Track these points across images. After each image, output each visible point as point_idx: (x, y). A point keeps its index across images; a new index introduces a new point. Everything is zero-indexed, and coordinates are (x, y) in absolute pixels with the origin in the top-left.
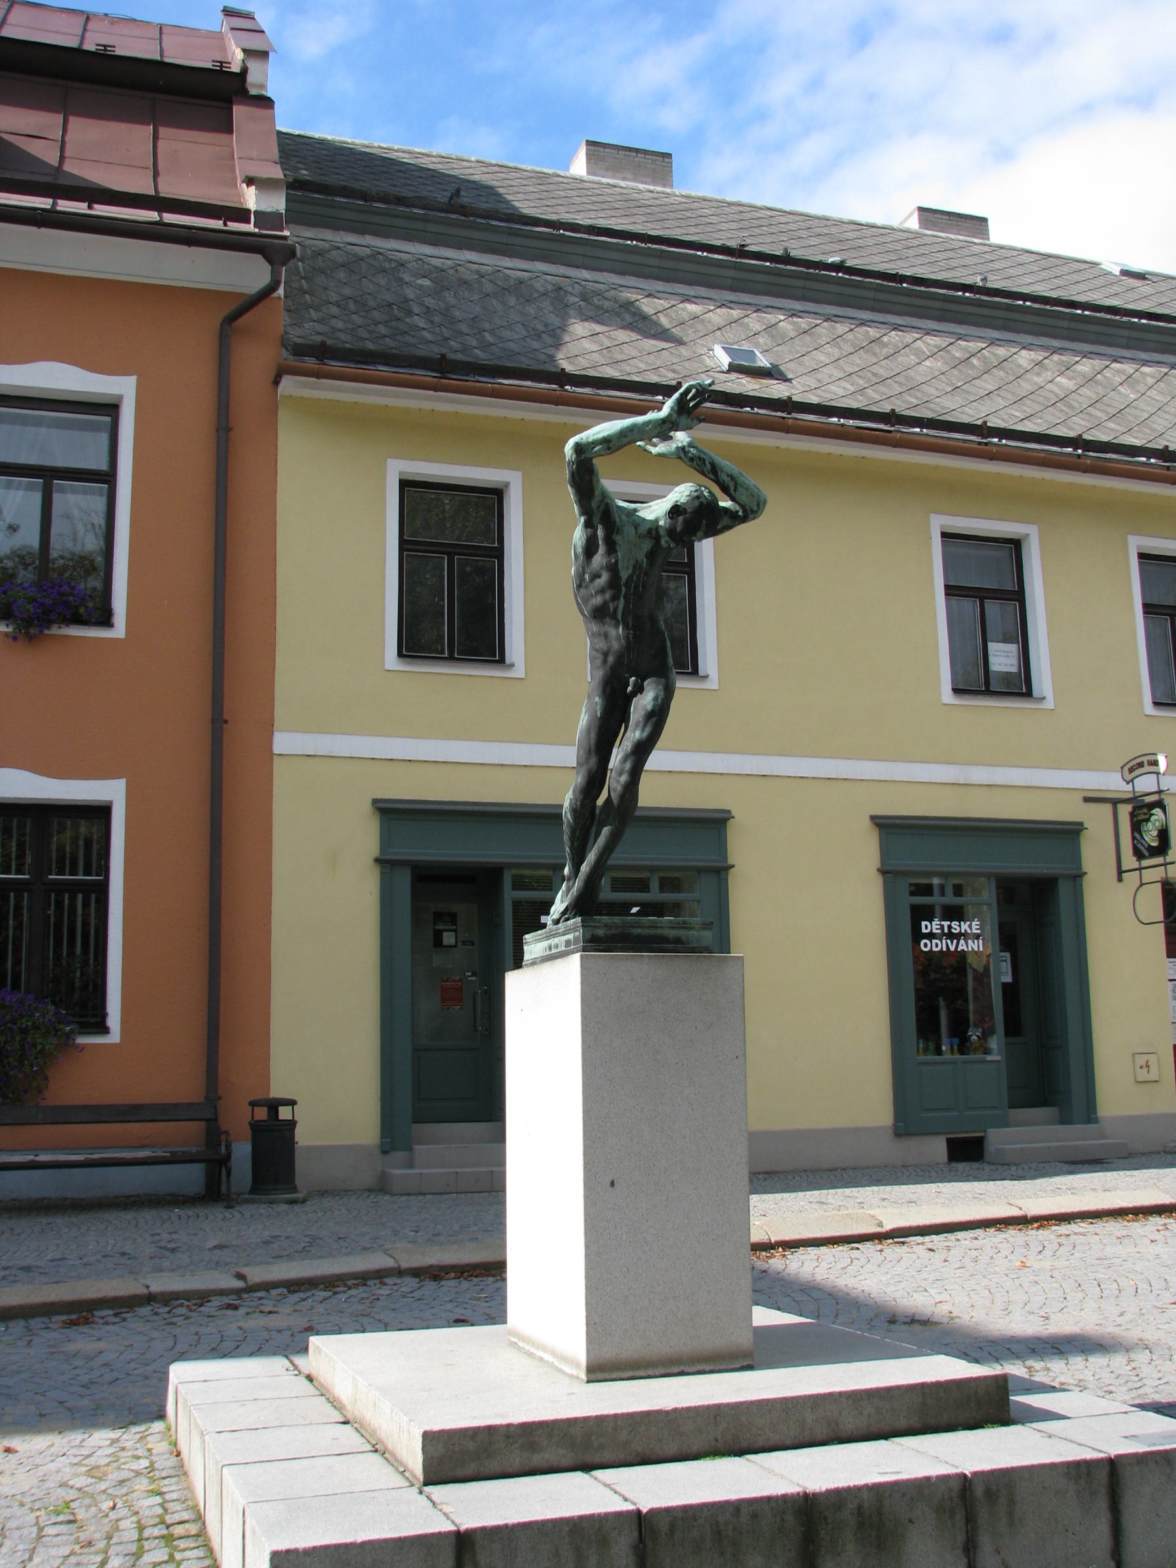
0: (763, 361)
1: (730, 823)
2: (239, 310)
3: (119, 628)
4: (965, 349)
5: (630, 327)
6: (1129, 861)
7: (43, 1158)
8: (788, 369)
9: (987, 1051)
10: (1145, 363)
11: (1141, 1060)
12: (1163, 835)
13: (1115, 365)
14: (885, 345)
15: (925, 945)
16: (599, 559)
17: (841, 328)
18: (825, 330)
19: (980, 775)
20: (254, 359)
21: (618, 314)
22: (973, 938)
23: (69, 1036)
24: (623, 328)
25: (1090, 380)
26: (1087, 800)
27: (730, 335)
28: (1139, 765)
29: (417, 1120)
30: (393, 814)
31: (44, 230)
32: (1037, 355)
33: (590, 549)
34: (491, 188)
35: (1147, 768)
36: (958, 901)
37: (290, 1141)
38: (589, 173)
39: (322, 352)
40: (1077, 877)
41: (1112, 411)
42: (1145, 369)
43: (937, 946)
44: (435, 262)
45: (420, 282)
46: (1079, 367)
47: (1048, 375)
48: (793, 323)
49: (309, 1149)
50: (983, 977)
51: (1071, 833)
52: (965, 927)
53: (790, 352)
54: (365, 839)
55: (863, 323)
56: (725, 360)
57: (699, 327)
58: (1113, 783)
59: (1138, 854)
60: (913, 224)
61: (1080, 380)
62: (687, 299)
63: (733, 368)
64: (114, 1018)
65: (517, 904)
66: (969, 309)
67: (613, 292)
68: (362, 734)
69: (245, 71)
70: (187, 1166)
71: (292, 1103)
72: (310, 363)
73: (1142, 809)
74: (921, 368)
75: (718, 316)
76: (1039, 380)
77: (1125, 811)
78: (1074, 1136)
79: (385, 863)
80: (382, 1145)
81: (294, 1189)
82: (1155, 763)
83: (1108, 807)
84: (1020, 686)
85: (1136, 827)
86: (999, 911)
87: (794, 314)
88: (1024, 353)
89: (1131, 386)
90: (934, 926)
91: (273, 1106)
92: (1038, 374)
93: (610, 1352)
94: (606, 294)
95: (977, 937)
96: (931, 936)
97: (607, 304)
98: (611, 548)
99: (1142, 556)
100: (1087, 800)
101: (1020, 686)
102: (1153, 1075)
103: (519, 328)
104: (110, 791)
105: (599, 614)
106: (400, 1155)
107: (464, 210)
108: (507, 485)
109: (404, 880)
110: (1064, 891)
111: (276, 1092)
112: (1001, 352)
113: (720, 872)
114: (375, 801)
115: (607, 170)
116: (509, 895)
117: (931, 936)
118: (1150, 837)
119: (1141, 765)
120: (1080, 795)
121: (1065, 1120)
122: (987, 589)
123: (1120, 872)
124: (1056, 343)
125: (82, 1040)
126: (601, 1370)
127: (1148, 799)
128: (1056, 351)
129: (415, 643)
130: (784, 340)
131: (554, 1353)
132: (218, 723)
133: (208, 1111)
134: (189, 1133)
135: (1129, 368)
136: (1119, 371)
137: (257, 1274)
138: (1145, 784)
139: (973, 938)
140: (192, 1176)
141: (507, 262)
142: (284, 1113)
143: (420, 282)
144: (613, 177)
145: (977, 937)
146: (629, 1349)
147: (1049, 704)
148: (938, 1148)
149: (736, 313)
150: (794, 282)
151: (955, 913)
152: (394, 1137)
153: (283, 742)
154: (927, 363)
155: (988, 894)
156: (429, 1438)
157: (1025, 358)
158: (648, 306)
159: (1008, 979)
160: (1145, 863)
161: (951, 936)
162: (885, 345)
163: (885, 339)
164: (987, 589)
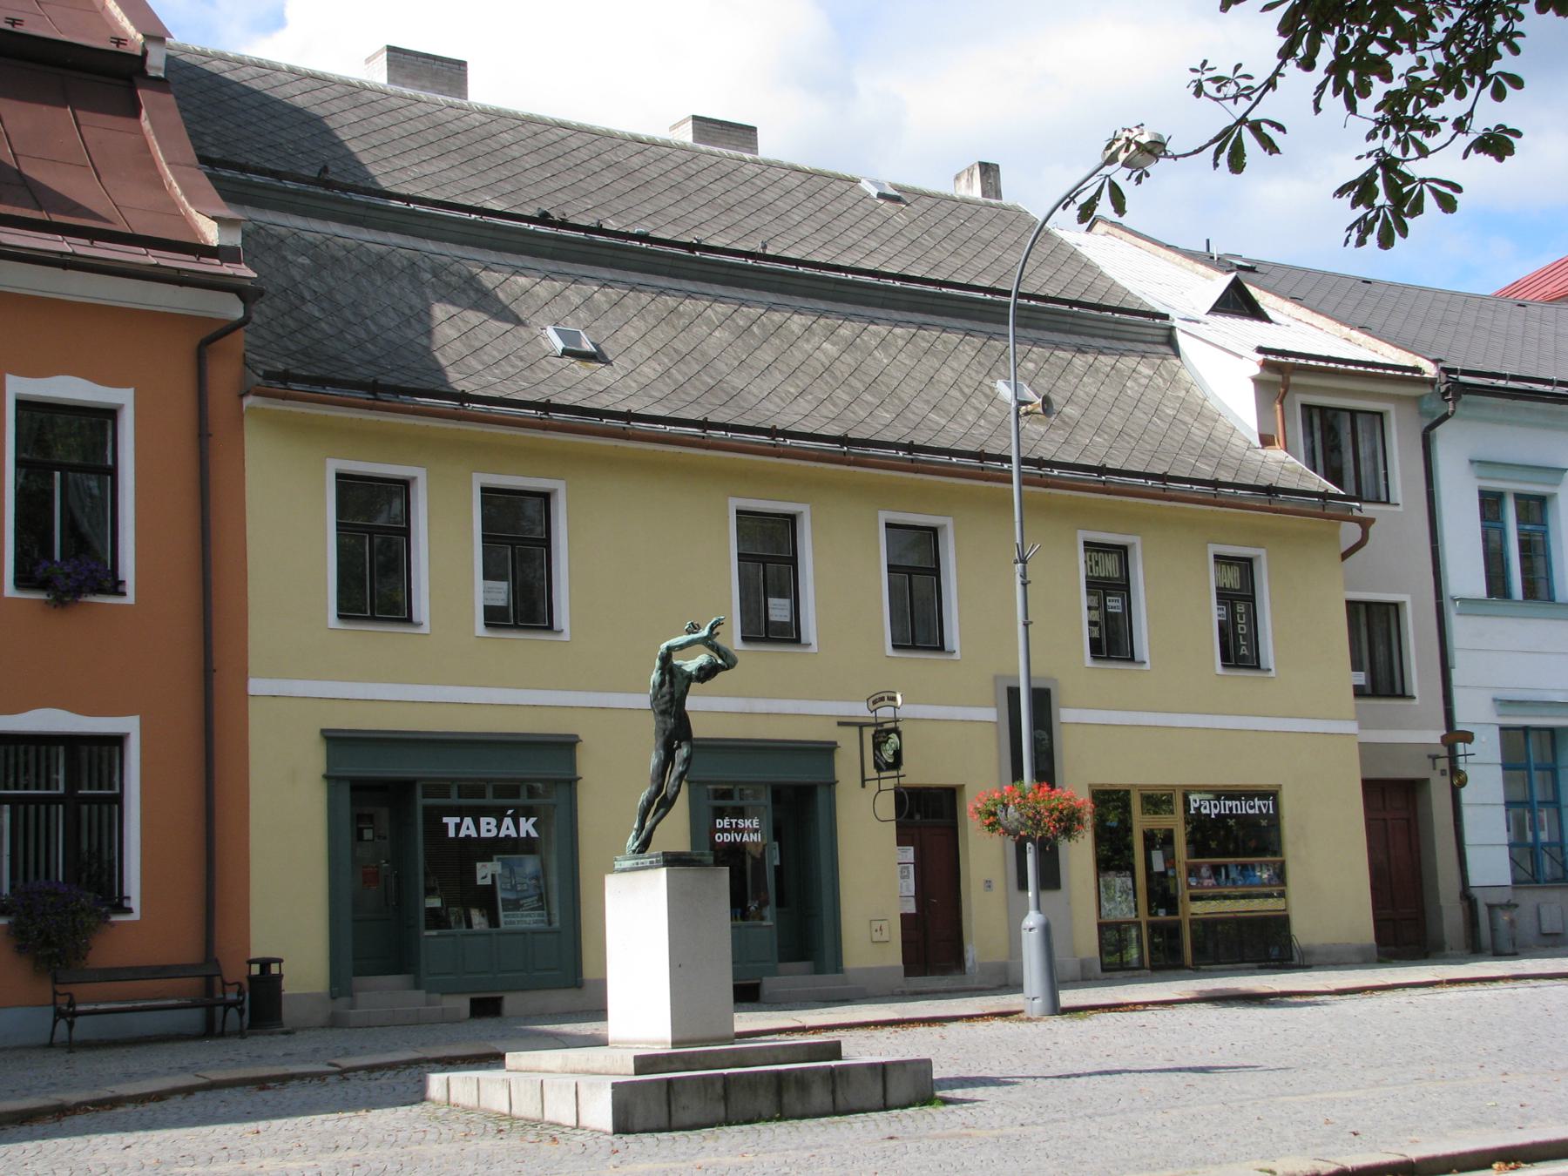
0: (588, 347)
1: (579, 746)
2: (213, 336)
3: (130, 598)
4: (747, 317)
5: (475, 307)
6: (871, 772)
7: (101, 1007)
8: (609, 349)
9: (762, 919)
10: (897, 324)
11: (876, 925)
12: (898, 754)
13: (872, 327)
14: (681, 315)
15: (721, 838)
16: (666, 689)
17: (645, 298)
18: (634, 301)
19: (761, 705)
20: (224, 373)
21: (464, 291)
22: (752, 831)
23: (108, 917)
24: (471, 308)
25: (850, 345)
26: (840, 724)
27: (556, 310)
28: (877, 700)
29: (356, 974)
30: (336, 741)
31: (70, 272)
32: (805, 320)
33: (662, 684)
34: (319, 119)
35: (886, 702)
36: (741, 803)
37: (279, 989)
38: (391, 80)
39: (285, 377)
40: (831, 785)
41: (868, 380)
42: (898, 331)
43: (727, 838)
44: (309, 236)
45: (300, 260)
46: (842, 331)
47: (816, 340)
48: (606, 295)
49: (293, 996)
50: (759, 863)
51: (826, 751)
52: (748, 823)
53: (606, 328)
54: (315, 760)
55: (662, 291)
56: (559, 345)
57: (530, 301)
58: (860, 710)
59: (878, 768)
60: (686, 136)
61: (842, 346)
62: (517, 271)
63: (565, 353)
64: (135, 903)
65: (426, 808)
66: (750, 274)
67: (456, 266)
68: (312, 679)
69: (145, 53)
70: (189, 1011)
71: (280, 961)
72: (278, 387)
73: (882, 733)
74: (712, 340)
75: (544, 289)
76: (808, 347)
77: (869, 733)
78: (826, 981)
79: (331, 779)
80: (331, 992)
81: (281, 1025)
82: (894, 699)
83: (856, 729)
84: (789, 634)
85: (877, 746)
86: (774, 810)
87: (604, 285)
88: (796, 317)
89: (885, 350)
90: (723, 823)
91: (265, 964)
92: (808, 341)
93: (679, 1037)
94: (452, 269)
95: (756, 831)
96: (723, 830)
97: (454, 279)
98: (672, 684)
99: (888, 525)
100: (840, 724)
101: (789, 634)
102: (885, 937)
103: (391, 314)
104: (128, 725)
105: (663, 713)
106: (343, 1001)
107: (329, 185)
108: (414, 478)
109: (345, 791)
110: (821, 794)
111: (256, 953)
112: (777, 317)
113: (571, 783)
114: (323, 731)
115: (407, 77)
116: (421, 802)
117: (723, 830)
118: (888, 754)
119: (882, 699)
120: (835, 721)
121: (818, 970)
122: (769, 556)
123: (864, 781)
124: (822, 305)
125: (114, 918)
126: (675, 1044)
127: (887, 726)
128: (822, 314)
129: (350, 609)
130: (598, 314)
131: (647, 1042)
132: (208, 672)
133: (208, 968)
134: (192, 984)
135: (882, 329)
136: (875, 334)
137: (347, 1062)
138: (885, 713)
139: (752, 831)
140: (195, 1017)
141: (366, 235)
142: (274, 969)
143: (300, 260)
144: (413, 87)
145: (756, 831)
146: (688, 1035)
147: (814, 648)
148: (462, 1004)
149: (558, 285)
150: (605, 252)
151: (740, 813)
152: (339, 984)
153: (256, 686)
154: (717, 334)
155: (766, 799)
156: (637, 1058)
157: (797, 322)
158: (489, 279)
159: (777, 862)
160: (883, 774)
161: (738, 831)
162: (681, 315)
163: (681, 308)
164: (769, 556)
